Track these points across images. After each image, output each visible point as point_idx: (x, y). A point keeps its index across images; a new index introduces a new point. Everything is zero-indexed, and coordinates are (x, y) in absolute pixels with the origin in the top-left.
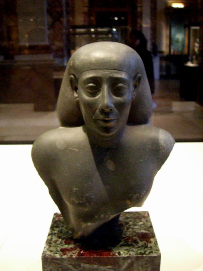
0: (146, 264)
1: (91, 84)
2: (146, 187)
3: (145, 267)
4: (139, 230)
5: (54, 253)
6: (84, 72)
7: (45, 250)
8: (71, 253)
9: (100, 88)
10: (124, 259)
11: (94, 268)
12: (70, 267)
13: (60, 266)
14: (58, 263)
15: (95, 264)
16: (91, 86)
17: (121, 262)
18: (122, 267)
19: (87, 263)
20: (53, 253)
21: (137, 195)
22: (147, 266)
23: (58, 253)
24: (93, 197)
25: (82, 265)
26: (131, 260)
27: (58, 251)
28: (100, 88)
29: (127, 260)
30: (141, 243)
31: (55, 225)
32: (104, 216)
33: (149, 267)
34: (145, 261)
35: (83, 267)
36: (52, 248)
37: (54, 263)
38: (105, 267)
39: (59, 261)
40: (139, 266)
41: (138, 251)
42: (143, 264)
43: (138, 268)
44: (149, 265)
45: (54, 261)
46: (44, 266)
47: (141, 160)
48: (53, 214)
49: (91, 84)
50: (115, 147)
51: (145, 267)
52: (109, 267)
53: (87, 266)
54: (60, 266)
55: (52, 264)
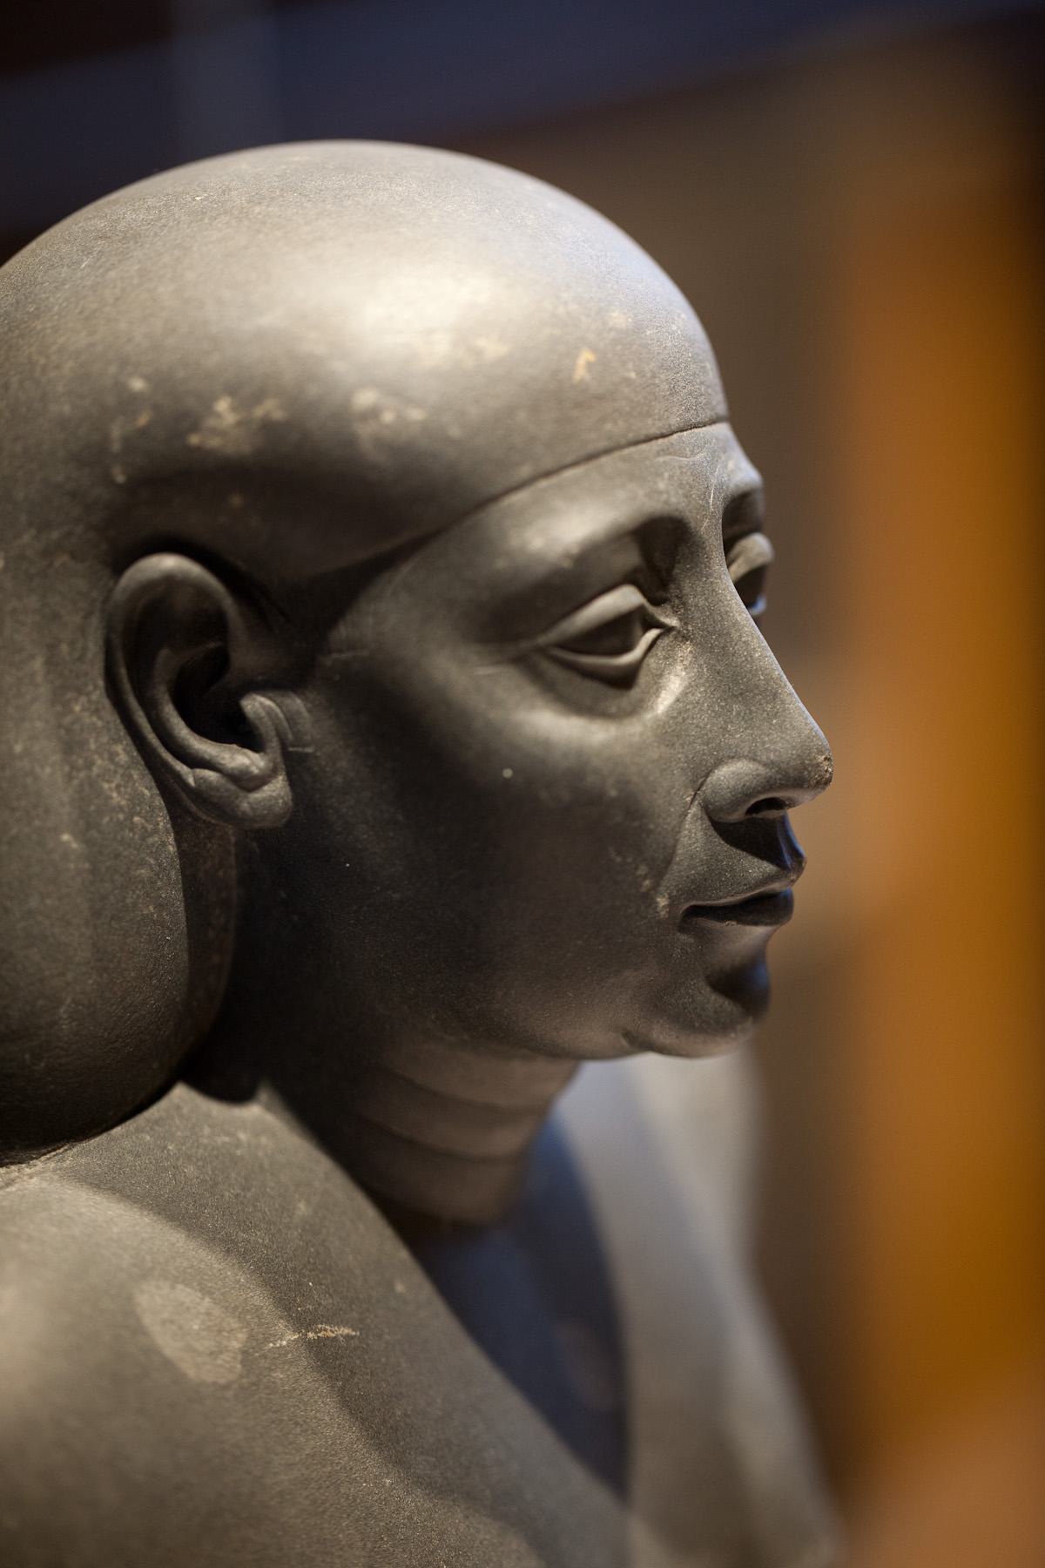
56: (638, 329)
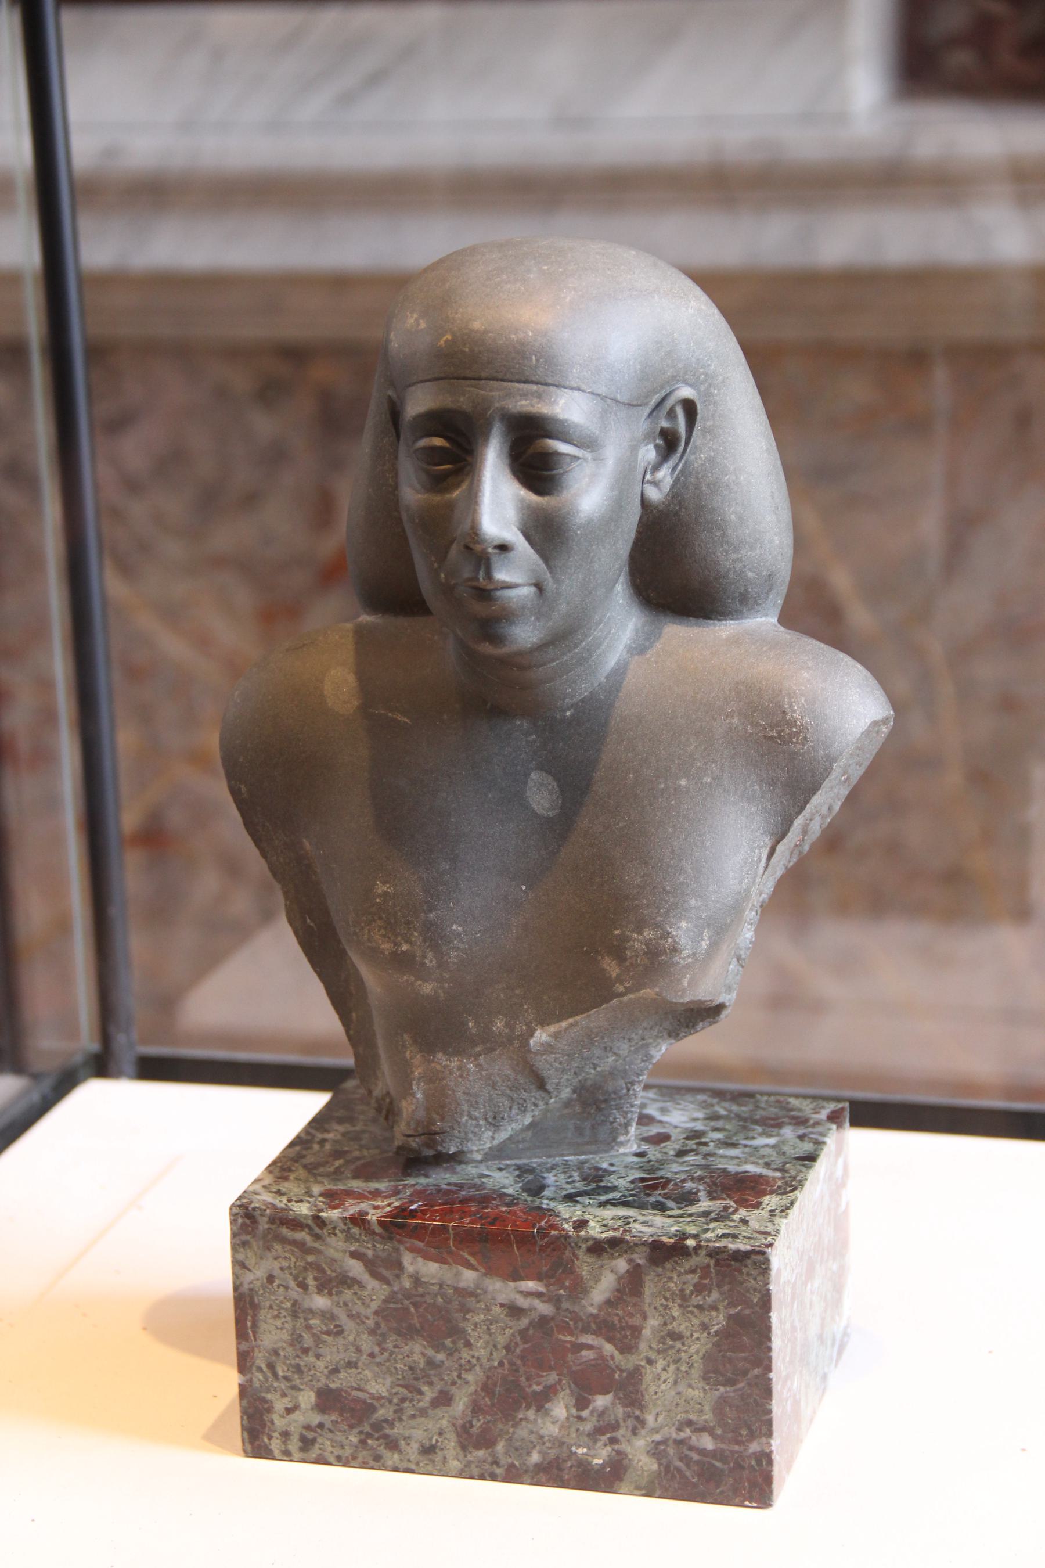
0: (699, 1289)
1: (438, 442)
2: (693, 902)
3: (699, 1307)
4: (735, 1161)
5: (289, 1201)
6: (413, 388)
7: (257, 1187)
8: (364, 1206)
9: (469, 459)
10: (598, 1248)
11: (462, 1285)
12: (356, 1268)
13: (310, 1258)
14: (301, 1245)
15: (469, 1266)
16: (433, 449)
17: (585, 1265)
18: (586, 1292)
19: (427, 1257)
20: (284, 1199)
21: (648, 934)
22: (709, 1300)
23: (309, 1202)
24: (454, 927)
25: (411, 1263)
26: (630, 1261)
27: (311, 1196)
28: (469, 459)
29: (612, 1257)
30: (705, 1204)
31: (341, 1113)
32: (507, 1025)
33: (714, 1308)
34: (693, 1271)
35: (411, 1276)
36: (284, 1186)
37: (283, 1240)
38: (512, 1284)
39: (302, 1235)
40: (666, 1299)
41: (672, 1226)
42: (689, 1288)
43: (666, 1307)
44: (715, 1295)
45: (284, 1231)
46: (240, 1257)
47: (683, 782)
48: (790, 1484)
49: (438, 442)
50: (568, 714)
51: (699, 1307)
52: (531, 1285)
53: (430, 1269)
54: (310, 1258)
55: (278, 1247)
56: (486, 332)
